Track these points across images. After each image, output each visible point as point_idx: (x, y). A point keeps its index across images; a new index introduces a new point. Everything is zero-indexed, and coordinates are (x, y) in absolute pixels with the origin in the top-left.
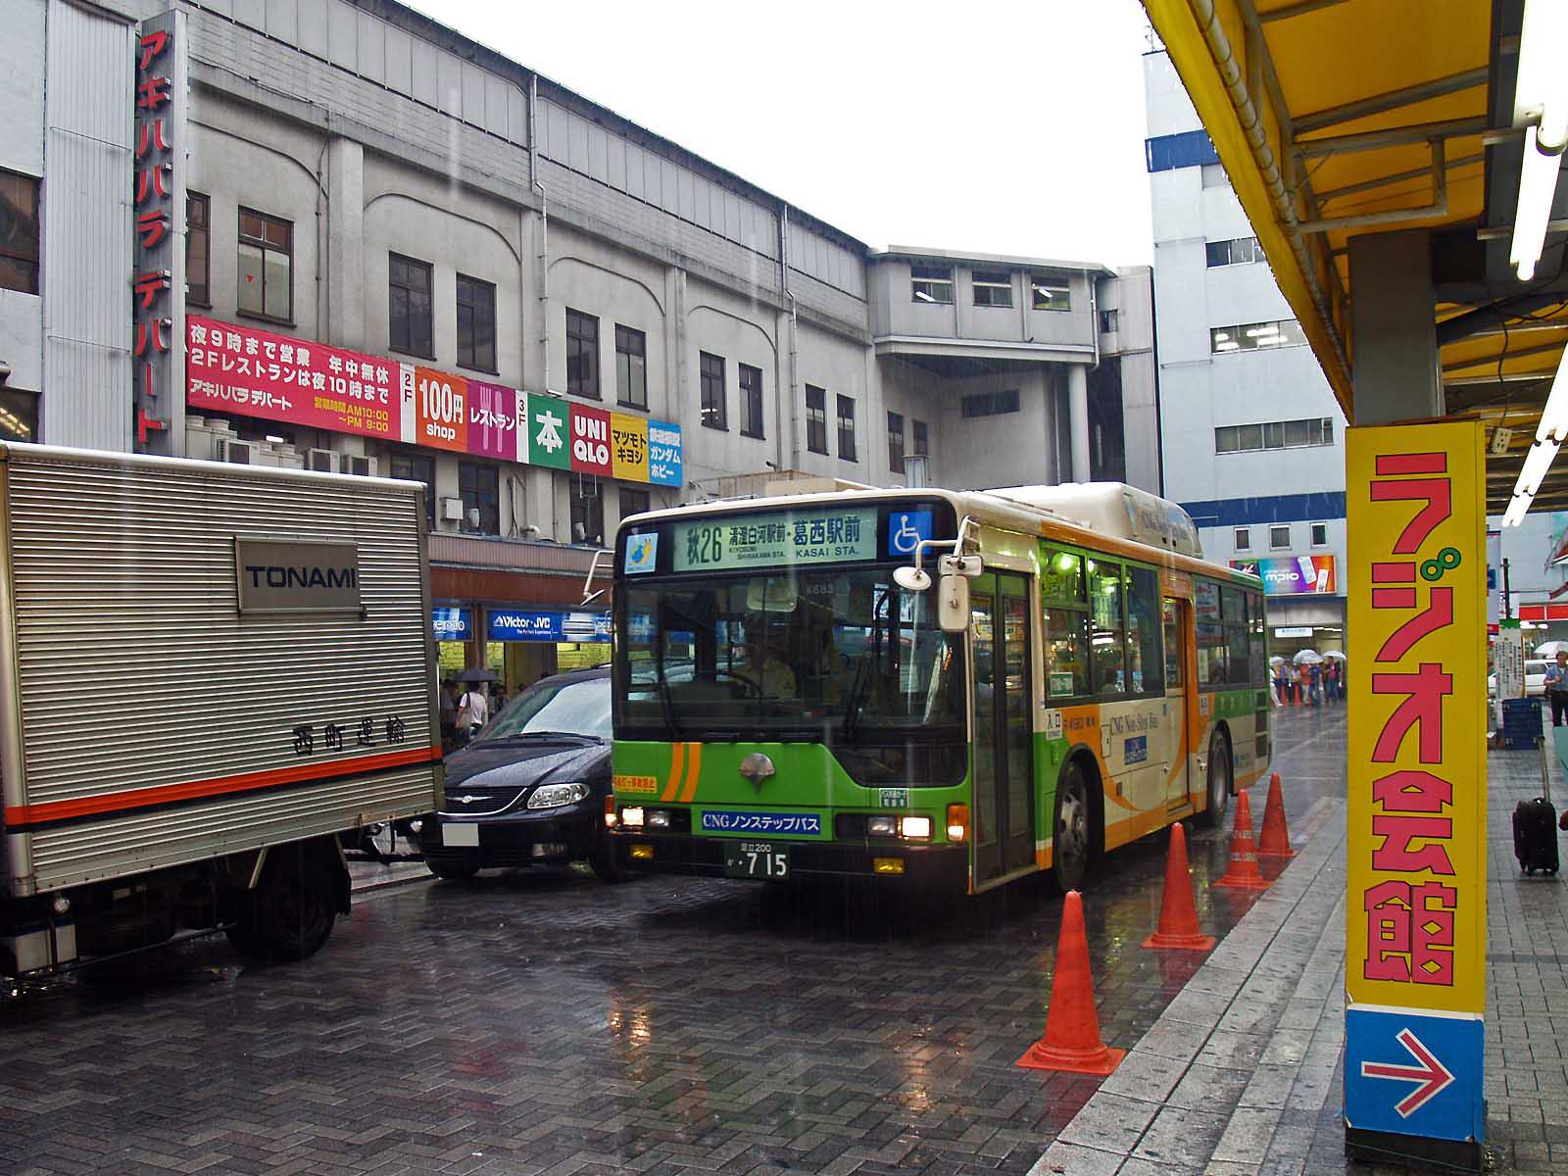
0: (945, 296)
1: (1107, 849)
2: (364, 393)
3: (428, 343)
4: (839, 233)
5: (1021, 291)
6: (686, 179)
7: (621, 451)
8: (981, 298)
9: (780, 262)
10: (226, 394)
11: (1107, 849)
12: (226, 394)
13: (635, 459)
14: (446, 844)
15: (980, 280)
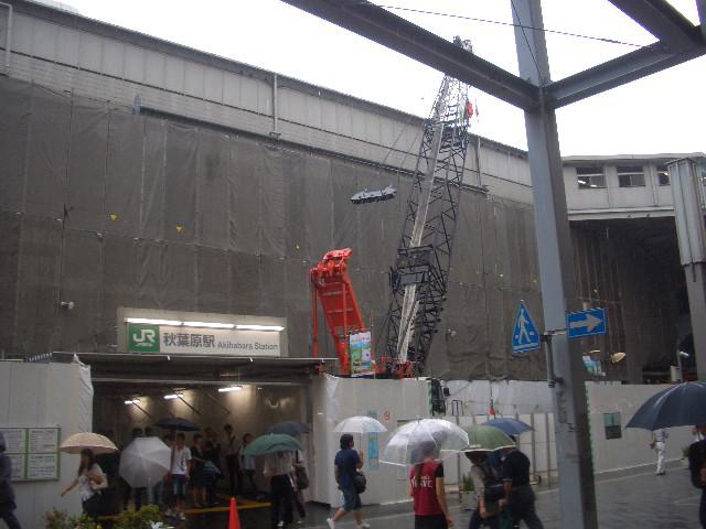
0: (601, 183)
1: (658, 40)
4: (512, 149)
5: (651, 176)
6: (346, 112)
8: (624, 182)
9: (478, 172)
11: (658, 40)
14: (556, 111)
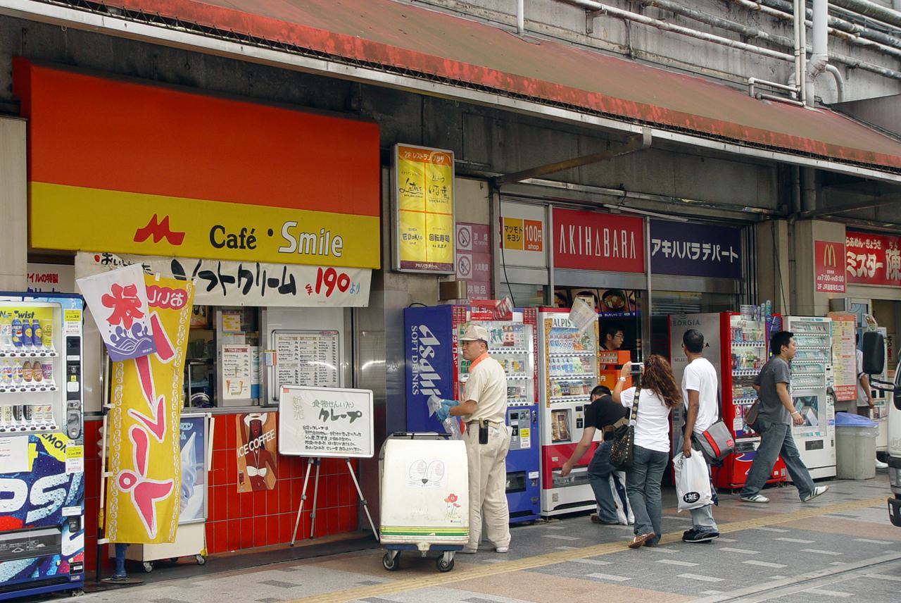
2: (473, 288)
3: (218, 59)
7: (509, 236)
10: (681, 254)
12: (681, 254)
13: (516, 239)
15: (788, 19)
